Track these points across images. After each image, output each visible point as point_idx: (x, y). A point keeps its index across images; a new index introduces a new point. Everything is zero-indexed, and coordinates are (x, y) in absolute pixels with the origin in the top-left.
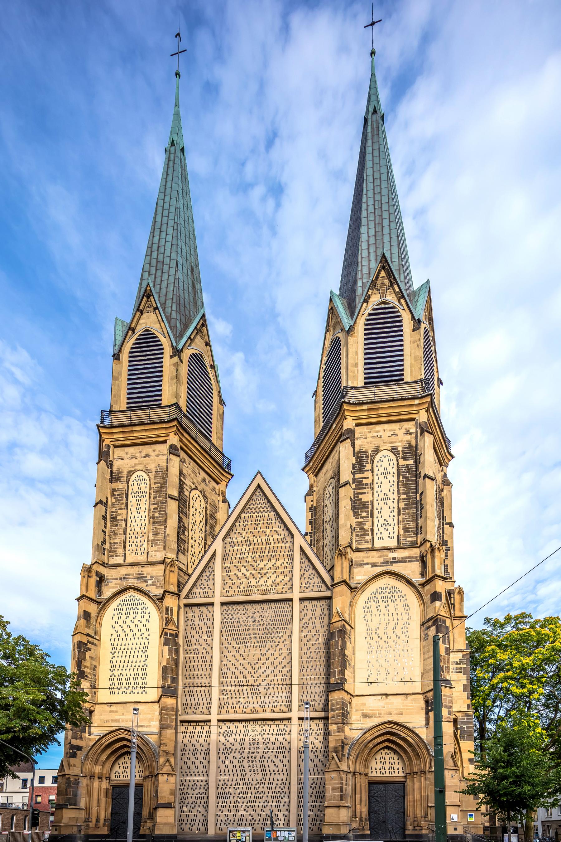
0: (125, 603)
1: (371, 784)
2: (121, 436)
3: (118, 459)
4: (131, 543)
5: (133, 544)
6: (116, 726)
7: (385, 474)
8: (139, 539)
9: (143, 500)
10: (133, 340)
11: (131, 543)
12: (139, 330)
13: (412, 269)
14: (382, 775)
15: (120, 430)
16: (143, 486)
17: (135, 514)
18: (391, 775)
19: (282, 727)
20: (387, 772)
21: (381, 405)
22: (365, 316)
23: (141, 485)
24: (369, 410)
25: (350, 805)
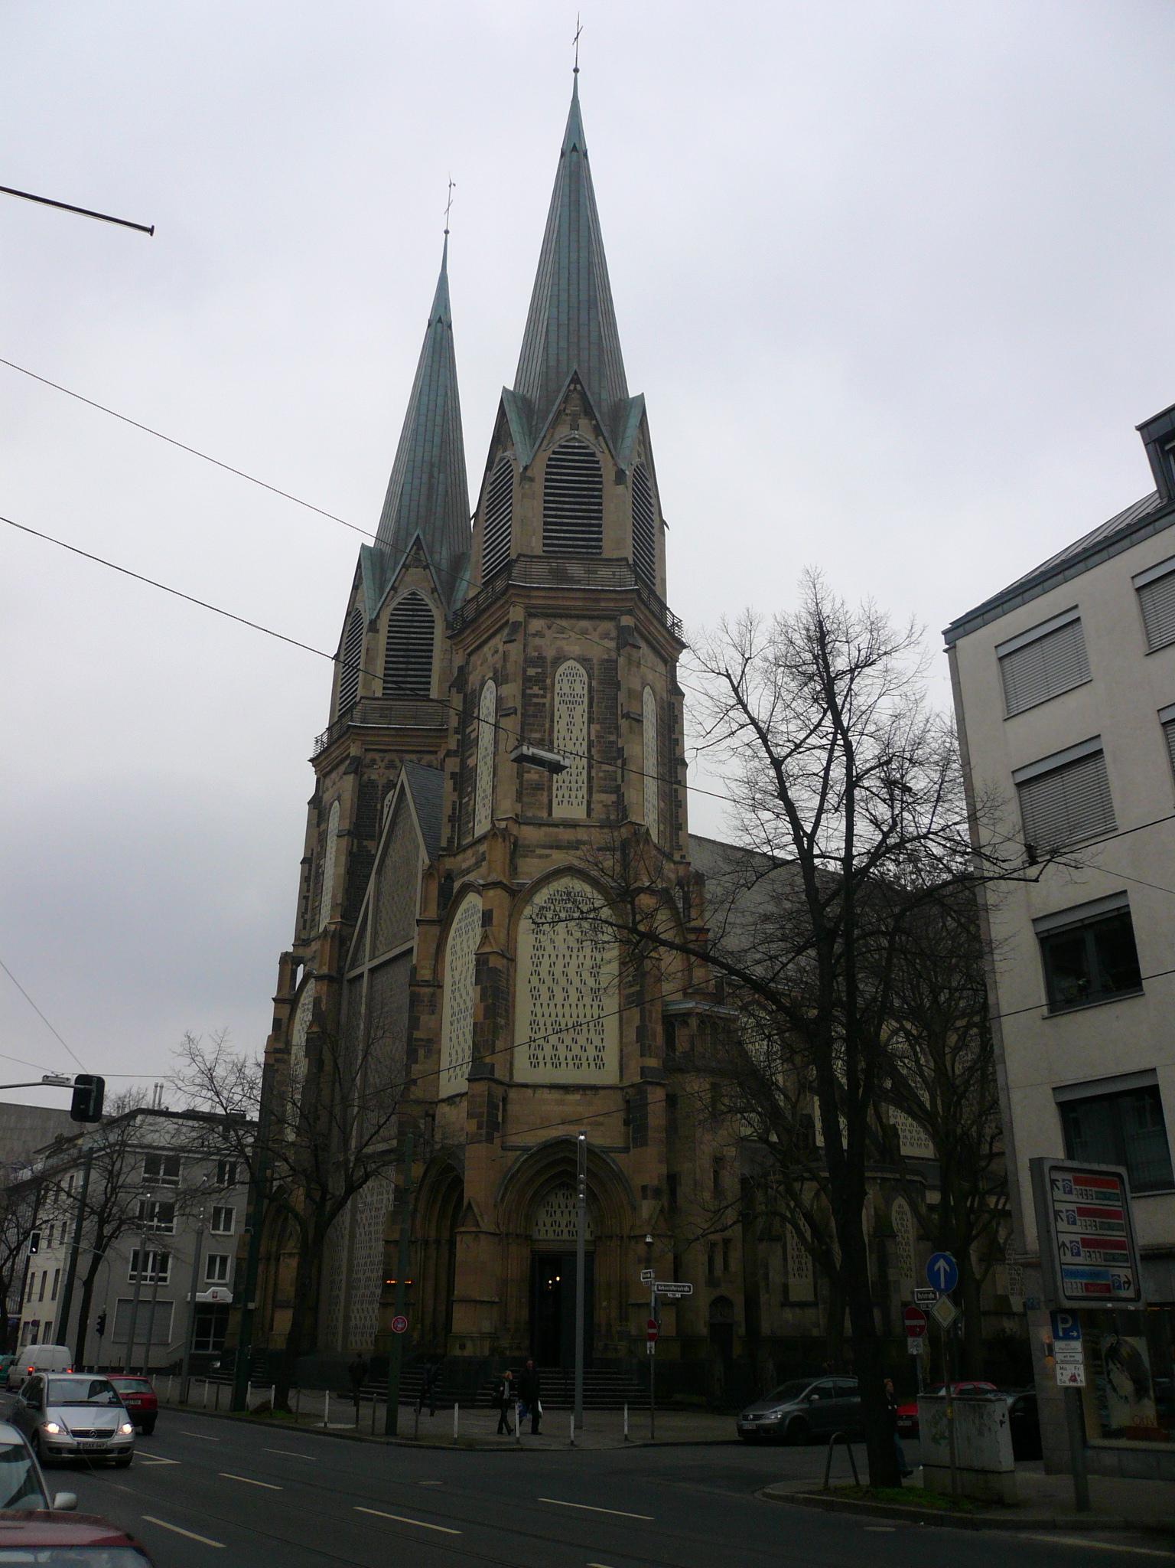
3: (534, 635)
10: (394, 604)
12: (404, 593)
17: (563, 732)
20: (566, 1231)
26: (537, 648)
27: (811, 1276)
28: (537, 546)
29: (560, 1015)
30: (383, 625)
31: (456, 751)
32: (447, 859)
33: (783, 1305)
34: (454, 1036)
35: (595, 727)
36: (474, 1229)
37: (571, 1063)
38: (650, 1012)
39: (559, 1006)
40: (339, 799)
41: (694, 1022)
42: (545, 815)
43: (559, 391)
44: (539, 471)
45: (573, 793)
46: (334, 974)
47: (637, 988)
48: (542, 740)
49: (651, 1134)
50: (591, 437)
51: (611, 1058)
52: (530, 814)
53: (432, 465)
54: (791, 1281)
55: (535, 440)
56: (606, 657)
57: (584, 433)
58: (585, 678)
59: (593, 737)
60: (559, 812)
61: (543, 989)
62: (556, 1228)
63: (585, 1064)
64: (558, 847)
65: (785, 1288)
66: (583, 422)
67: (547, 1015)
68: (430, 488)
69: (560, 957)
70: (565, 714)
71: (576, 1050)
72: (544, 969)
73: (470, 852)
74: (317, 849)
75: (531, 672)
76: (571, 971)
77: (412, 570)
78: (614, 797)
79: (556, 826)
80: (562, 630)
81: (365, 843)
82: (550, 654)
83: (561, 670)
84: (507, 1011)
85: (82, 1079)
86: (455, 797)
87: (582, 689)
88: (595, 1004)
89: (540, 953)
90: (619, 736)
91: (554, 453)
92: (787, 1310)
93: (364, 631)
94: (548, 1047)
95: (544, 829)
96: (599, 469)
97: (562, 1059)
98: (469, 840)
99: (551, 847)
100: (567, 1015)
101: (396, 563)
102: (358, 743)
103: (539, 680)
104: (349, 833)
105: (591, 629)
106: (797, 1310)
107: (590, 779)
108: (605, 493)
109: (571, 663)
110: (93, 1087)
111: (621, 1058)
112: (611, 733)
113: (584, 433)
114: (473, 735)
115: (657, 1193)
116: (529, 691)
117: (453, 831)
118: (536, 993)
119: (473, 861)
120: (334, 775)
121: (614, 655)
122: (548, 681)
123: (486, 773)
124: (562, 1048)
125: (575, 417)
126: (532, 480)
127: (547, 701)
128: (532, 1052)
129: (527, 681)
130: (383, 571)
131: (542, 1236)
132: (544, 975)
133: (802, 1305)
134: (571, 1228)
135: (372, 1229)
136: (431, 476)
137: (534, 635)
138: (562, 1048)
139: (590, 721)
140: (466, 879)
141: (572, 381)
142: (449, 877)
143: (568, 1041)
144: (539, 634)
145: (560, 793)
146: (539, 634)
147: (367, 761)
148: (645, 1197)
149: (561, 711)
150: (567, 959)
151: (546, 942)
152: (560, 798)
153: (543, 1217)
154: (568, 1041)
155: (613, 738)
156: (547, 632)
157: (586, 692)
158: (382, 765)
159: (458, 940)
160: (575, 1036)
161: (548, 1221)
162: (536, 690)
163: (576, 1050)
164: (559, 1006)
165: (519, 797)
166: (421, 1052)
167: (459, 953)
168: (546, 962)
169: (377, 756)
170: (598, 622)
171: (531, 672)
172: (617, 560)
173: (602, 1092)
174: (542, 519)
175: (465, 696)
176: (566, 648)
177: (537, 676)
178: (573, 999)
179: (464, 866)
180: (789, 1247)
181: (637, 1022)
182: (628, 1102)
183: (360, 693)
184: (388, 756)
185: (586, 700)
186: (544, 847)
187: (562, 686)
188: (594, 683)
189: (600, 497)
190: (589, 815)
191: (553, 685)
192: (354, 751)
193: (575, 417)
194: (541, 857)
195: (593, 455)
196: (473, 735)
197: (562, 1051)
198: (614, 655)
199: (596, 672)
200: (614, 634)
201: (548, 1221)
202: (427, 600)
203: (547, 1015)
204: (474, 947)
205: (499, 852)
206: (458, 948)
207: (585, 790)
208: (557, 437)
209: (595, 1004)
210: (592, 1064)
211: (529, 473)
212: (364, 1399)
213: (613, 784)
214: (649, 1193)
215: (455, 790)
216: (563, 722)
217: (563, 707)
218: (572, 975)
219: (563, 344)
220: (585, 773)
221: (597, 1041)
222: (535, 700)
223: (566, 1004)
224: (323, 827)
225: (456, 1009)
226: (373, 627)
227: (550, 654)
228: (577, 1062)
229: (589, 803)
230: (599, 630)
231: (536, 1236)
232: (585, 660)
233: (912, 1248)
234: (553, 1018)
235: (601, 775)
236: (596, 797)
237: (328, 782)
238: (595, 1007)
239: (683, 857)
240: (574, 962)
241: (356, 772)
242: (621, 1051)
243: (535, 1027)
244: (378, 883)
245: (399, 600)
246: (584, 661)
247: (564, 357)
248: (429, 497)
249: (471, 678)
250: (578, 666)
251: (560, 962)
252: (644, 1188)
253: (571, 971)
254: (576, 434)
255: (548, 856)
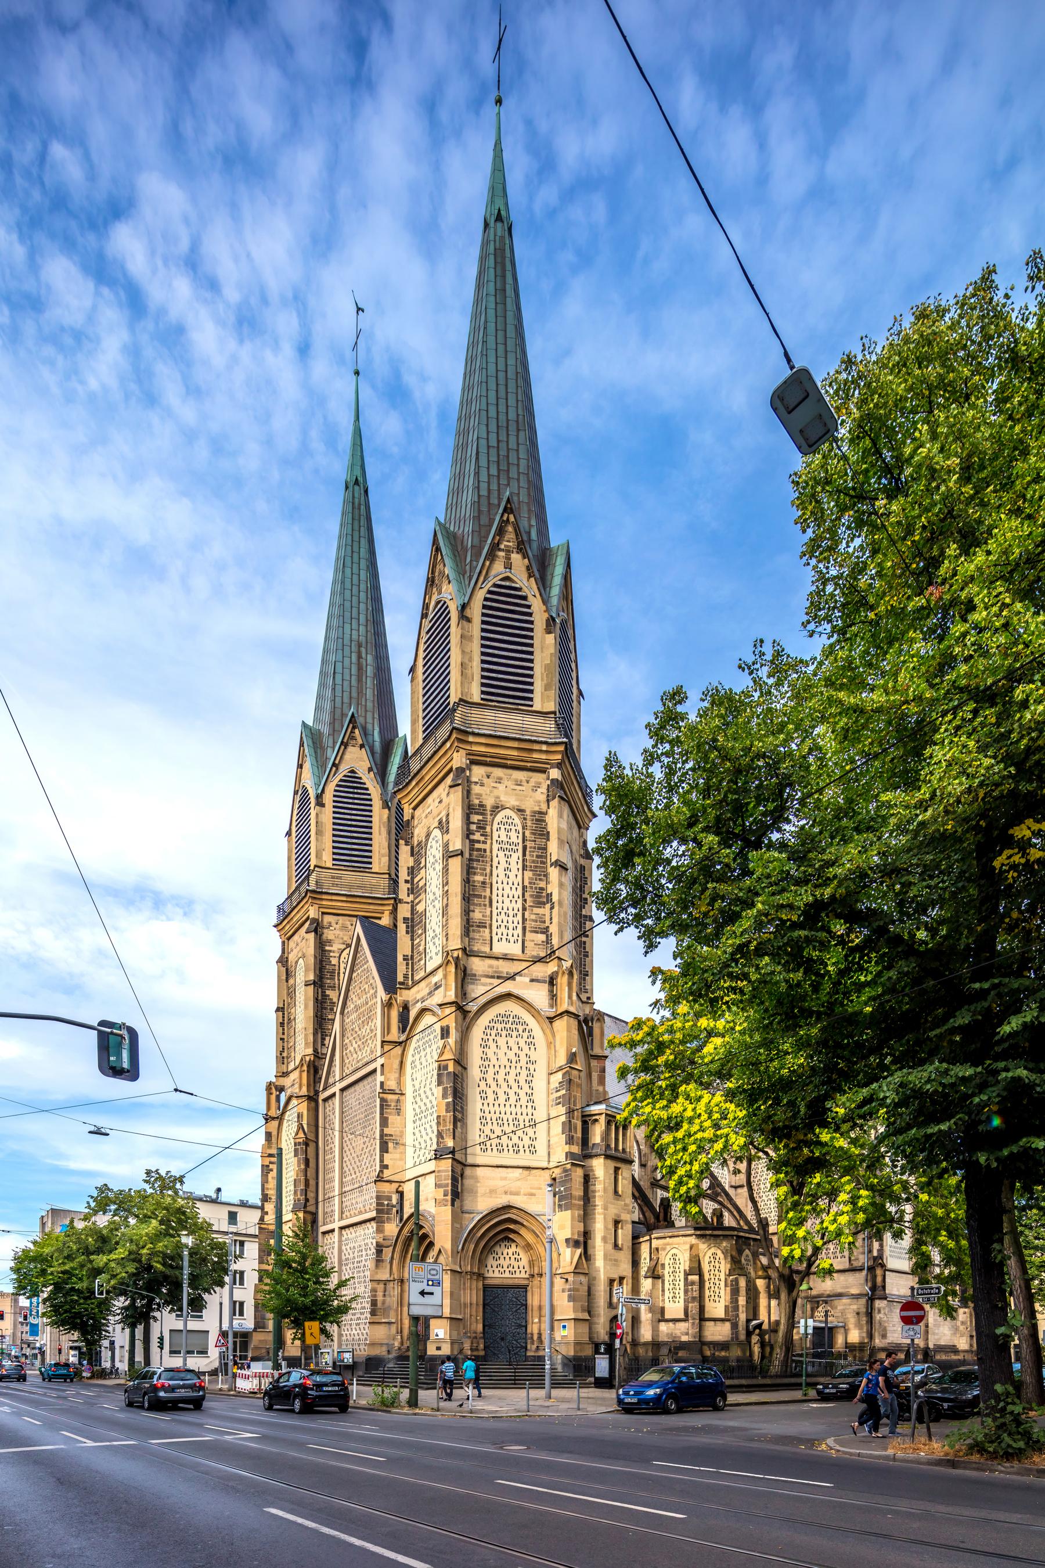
0: (500, 1019)
2: (515, 753)
4: (500, 922)
5: (503, 925)
7: (507, 849)
8: (511, 919)
9: (515, 856)
10: (336, 781)
11: (500, 922)
12: (344, 769)
15: (516, 744)
16: (513, 835)
17: (502, 876)
23: (505, 833)
24: (417, 784)
25: (393, 1320)
26: (479, 795)
27: (682, 1301)
30: (328, 798)
34: (417, 1131)
37: (511, 1150)
39: (502, 1106)
40: (304, 956)
42: (487, 949)
43: (491, 526)
46: (312, 1094)
53: (360, 646)
56: (537, 809)
60: (499, 948)
61: (489, 1092)
62: (500, 1269)
69: (502, 1067)
70: (503, 860)
73: (423, 984)
76: (511, 1078)
78: (543, 937)
79: (497, 958)
80: (499, 780)
83: (499, 818)
84: (462, 1108)
89: (486, 1063)
90: (547, 883)
96: (531, 615)
98: (422, 974)
101: (334, 743)
104: (314, 983)
106: (671, 1324)
114: (421, 884)
115: (576, 1244)
118: (484, 1095)
119: (427, 991)
120: (296, 937)
121: (544, 807)
122: (488, 829)
123: (435, 915)
131: (491, 1274)
132: (490, 1081)
133: (675, 1321)
134: (511, 1269)
135: (362, 1274)
136: (359, 657)
139: (524, 868)
142: (406, 1008)
145: (500, 931)
151: (490, 1055)
152: (500, 936)
155: (542, 884)
156: (485, 780)
159: (417, 1056)
164: (502, 1106)
166: (391, 1145)
167: (419, 1067)
168: (491, 1070)
170: (530, 774)
175: (412, 848)
178: (512, 1101)
179: (419, 997)
183: (313, 863)
187: (499, 834)
188: (527, 834)
190: (523, 952)
192: (313, 913)
195: (525, 598)
196: (421, 884)
198: (544, 807)
199: (529, 823)
201: (495, 1264)
203: (492, 1112)
206: (417, 1063)
215: (407, 932)
216: (501, 868)
217: (501, 854)
218: (511, 1082)
219: (494, 471)
223: (508, 1104)
224: (291, 981)
225: (418, 1111)
226: (320, 803)
227: (489, 803)
228: (516, 1149)
231: (487, 1275)
232: (519, 810)
235: (533, 917)
237: (292, 944)
238: (529, 1107)
240: (513, 1072)
243: (484, 1121)
244: (343, 1021)
246: (520, 811)
249: (416, 832)
250: (514, 816)
251: (502, 1072)
253: (511, 1078)
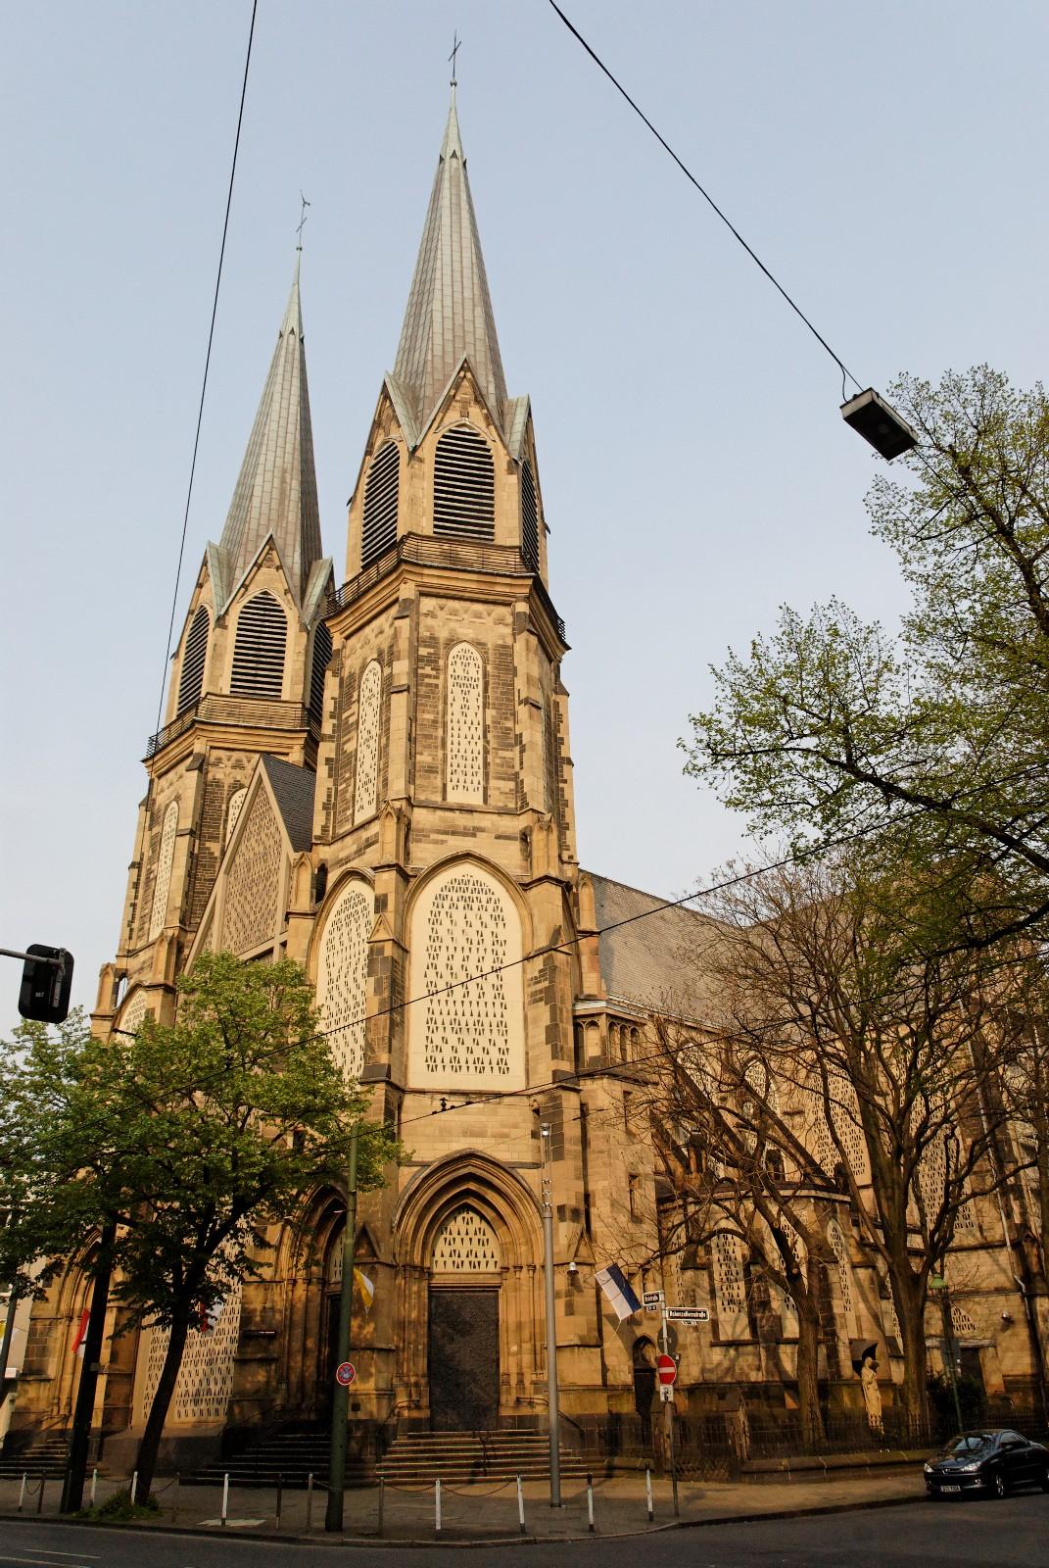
1: (434, 1293)
3: (426, 615)
4: (455, 767)
6: (459, 1145)
8: (469, 762)
10: (244, 602)
11: (455, 767)
12: (255, 591)
13: (508, 388)
14: (456, 1270)
17: (458, 716)
18: (473, 1270)
19: (839, 1123)
20: (466, 1264)
21: (426, 571)
22: (438, 437)
26: (429, 628)
28: (427, 527)
29: (460, 1013)
30: (233, 621)
31: (331, 737)
32: (321, 847)
33: (713, 1345)
35: (491, 713)
36: (369, 1260)
37: (472, 1067)
38: (561, 1010)
39: (459, 1003)
41: (603, 1022)
42: (438, 798)
43: (446, 380)
44: (428, 453)
45: (469, 778)
47: (547, 984)
48: (435, 721)
49: (567, 1146)
50: (482, 424)
51: (516, 1061)
52: (422, 797)
53: (284, 471)
54: (722, 1316)
55: (422, 424)
56: (500, 642)
57: (476, 419)
58: (480, 662)
59: (489, 722)
62: (456, 1258)
63: (488, 1068)
64: (454, 833)
65: (715, 1324)
66: (475, 411)
67: (445, 1012)
68: (283, 492)
69: (459, 949)
71: (478, 1052)
72: (441, 962)
73: (349, 840)
74: (148, 853)
75: (423, 651)
77: (263, 570)
78: (512, 785)
79: (451, 810)
81: (208, 844)
82: (443, 635)
83: (454, 652)
85: (35, 949)
86: (330, 783)
87: (476, 673)
88: (498, 1002)
89: (437, 944)
90: (516, 722)
91: (444, 436)
92: (718, 1350)
93: (211, 627)
94: (447, 1049)
95: (439, 813)
96: (490, 457)
97: (463, 1063)
98: (348, 827)
99: (446, 833)
100: (468, 1014)
102: (204, 740)
103: (432, 660)
105: (485, 614)
107: (486, 764)
108: (496, 481)
109: (464, 646)
110: (61, 960)
111: (527, 1061)
112: (506, 719)
113: (476, 419)
114: (352, 720)
116: (420, 671)
117: (327, 819)
119: (354, 848)
122: (441, 662)
123: (368, 756)
124: (462, 1049)
125: (465, 404)
126: (421, 461)
127: (440, 682)
128: (429, 1053)
129: (417, 661)
130: (231, 569)
132: (441, 968)
134: (472, 1258)
136: (283, 481)
137: (426, 615)
138: (462, 1049)
139: (485, 706)
140: (349, 865)
141: (462, 368)
143: (469, 1043)
144: (431, 614)
145: (455, 778)
146: (431, 614)
147: (212, 760)
148: (562, 1219)
149: (455, 694)
150: (466, 952)
153: (441, 1246)
154: (469, 1043)
155: (509, 724)
157: (480, 676)
158: (230, 764)
159: (337, 934)
160: (477, 1037)
161: (447, 1250)
162: (428, 670)
163: (478, 1052)
164: (459, 1003)
165: (411, 778)
167: (338, 947)
168: (443, 954)
169: (222, 754)
170: (491, 607)
171: (423, 651)
172: (510, 547)
173: (506, 1100)
174: (433, 501)
176: (460, 630)
177: (429, 656)
180: (716, 1276)
181: (546, 1020)
182: (537, 1111)
184: (236, 755)
185: (481, 684)
186: (439, 832)
187: (456, 669)
188: (489, 668)
189: (492, 485)
190: (485, 801)
191: (446, 666)
192: (199, 746)
193: (465, 404)
194: (436, 842)
197: (462, 1054)
198: (509, 641)
199: (491, 657)
200: (510, 620)
201: (447, 1250)
202: (279, 601)
203: (445, 1012)
204: (365, 936)
205: (388, 831)
207: (480, 776)
208: (446, 421)
209: (498, 1002)
210: (496, 1068)
211: (419, 454)
212: (590, 1389)
213: (513, 771)
214: (568, 1214)
215: (330, 776)
217: (457, 690)
220: (480, 757)
221: (500, 1043)
222: (427, 680)
223: (467, 1001)
226: (221, 621)
227: (443, 635)
228: (479, 1065)
229: (485, 789)
230: (494, 615)
232: (479, 644)
233: (848, 1277)
234: (452, 1016)
235: (498, 761)
236: (493, 783)
239: (571, 857)
240: (474, 956)
241: (200, 769)
242: (527, 1053)
243: (432, 1026)
245: (250, 598)
246: (479, 645)
247: (449, 348)
248: (281, 502)
250: (472, 649)
251: (459, 956)
252: (561, 1209)
254: (466, 421)
255: (443, 842)
